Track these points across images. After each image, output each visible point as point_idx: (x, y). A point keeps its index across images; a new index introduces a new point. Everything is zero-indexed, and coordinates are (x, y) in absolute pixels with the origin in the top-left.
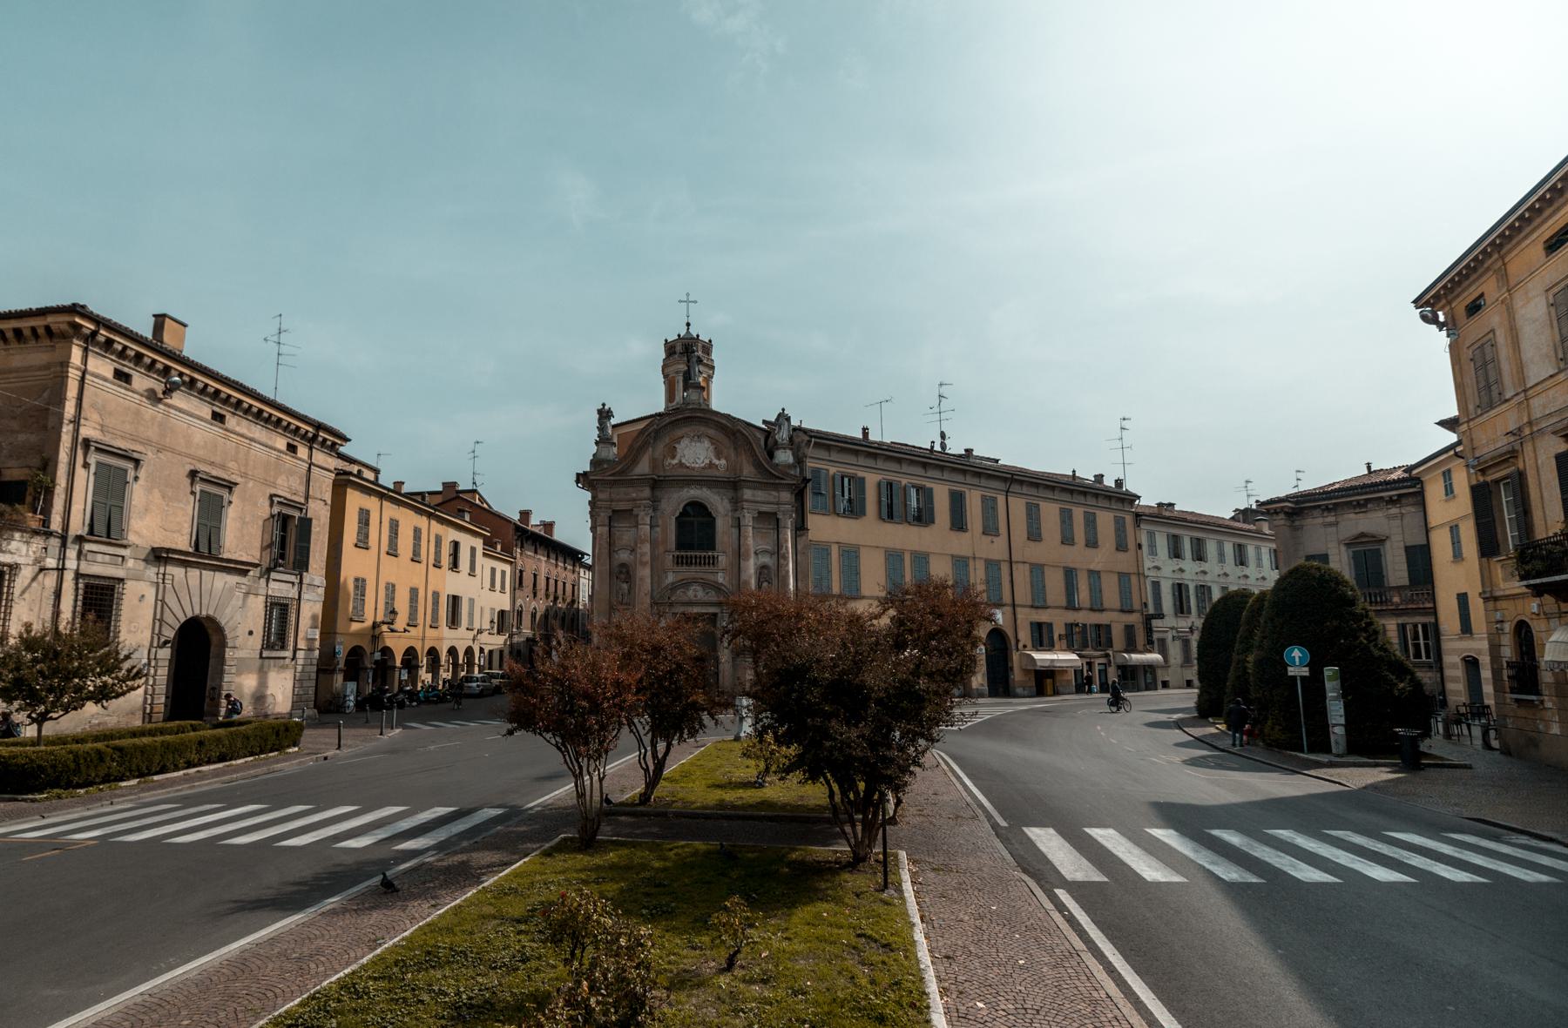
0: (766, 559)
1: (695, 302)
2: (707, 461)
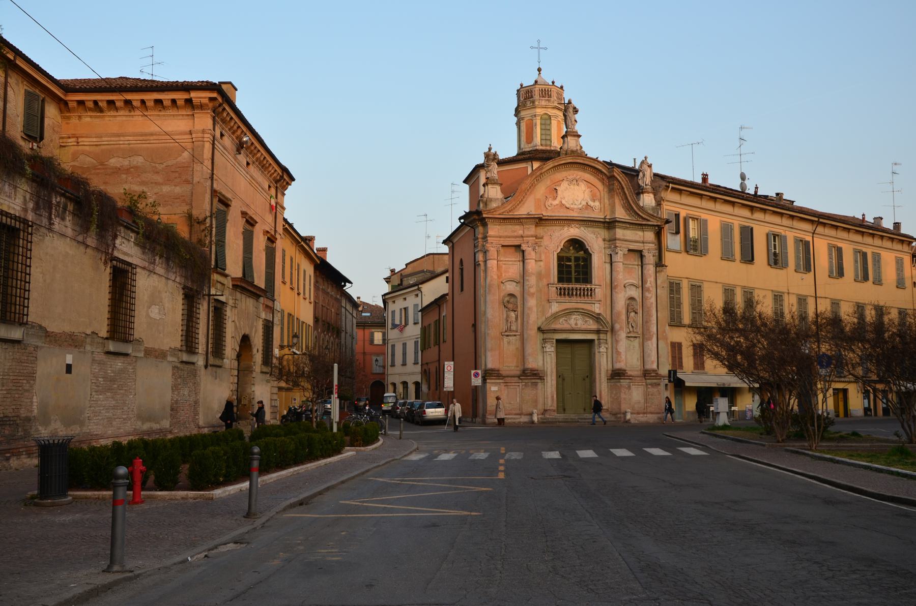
0: (635, 293)
2: (584, 203)
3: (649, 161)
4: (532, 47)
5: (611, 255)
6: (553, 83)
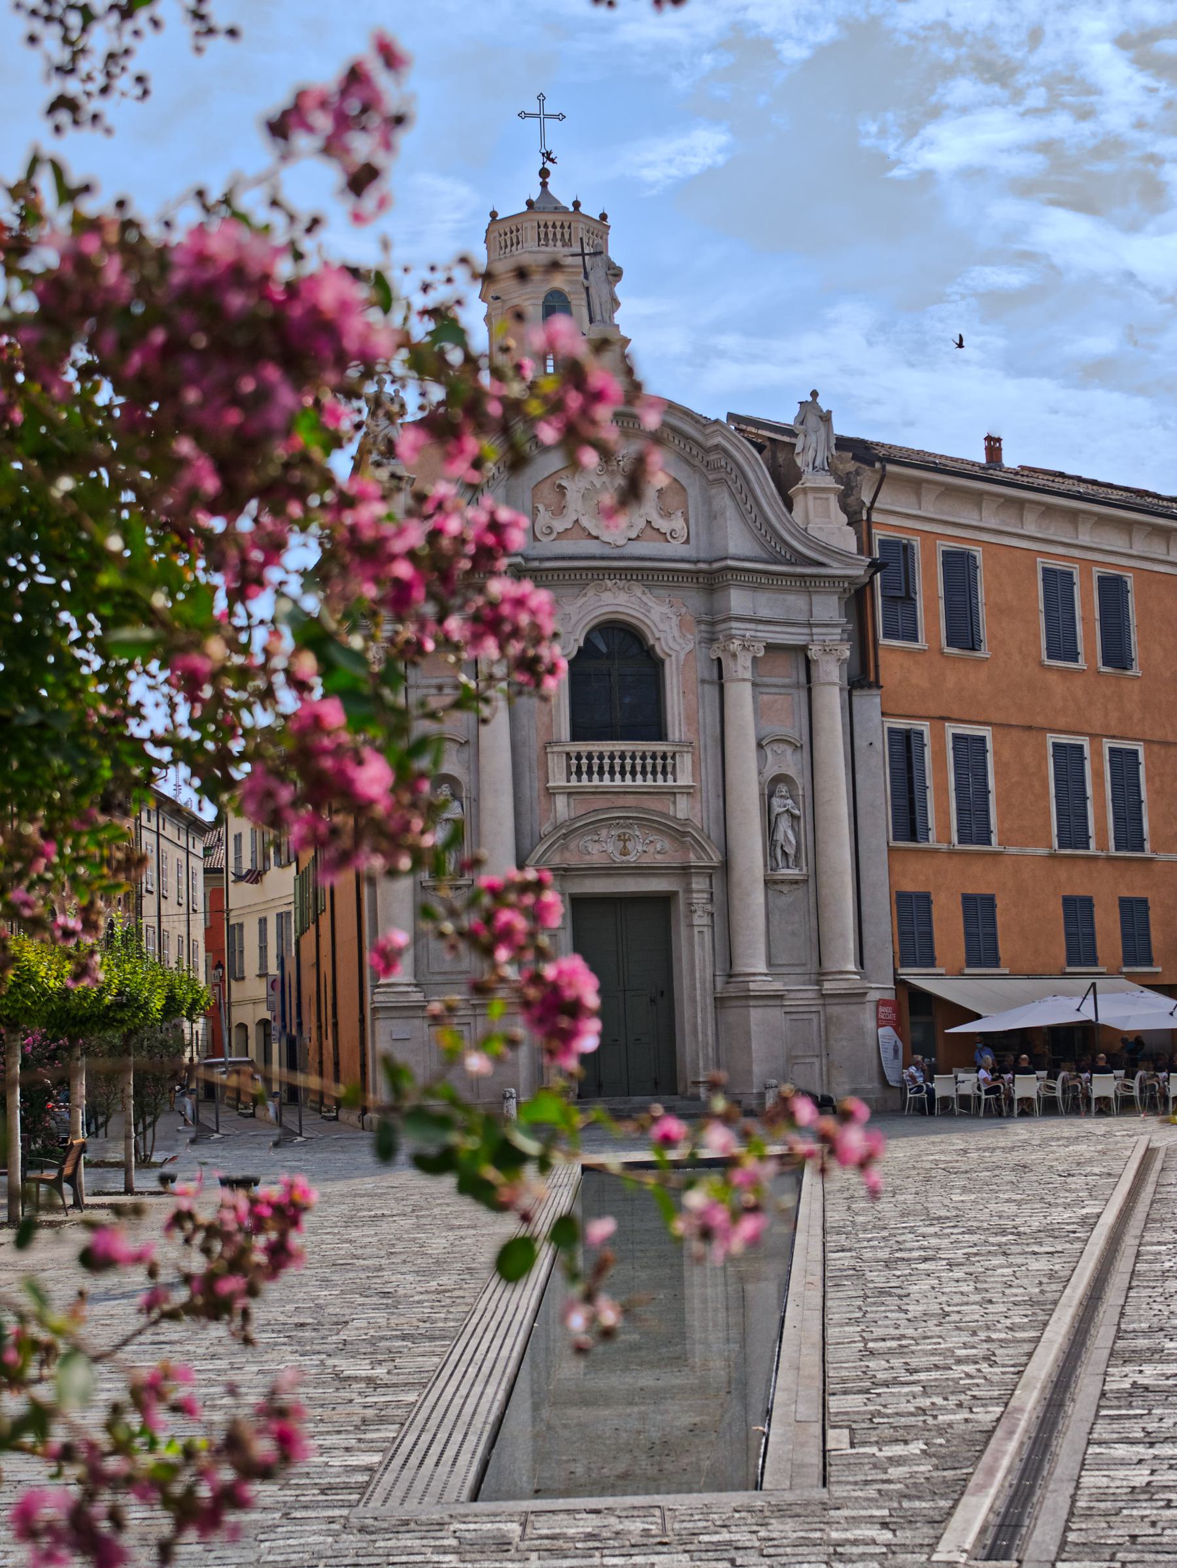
1: (561, 117)
3: (824, 404)
4: (523, 115)
5: (719, 660)
6: (577, 204)
